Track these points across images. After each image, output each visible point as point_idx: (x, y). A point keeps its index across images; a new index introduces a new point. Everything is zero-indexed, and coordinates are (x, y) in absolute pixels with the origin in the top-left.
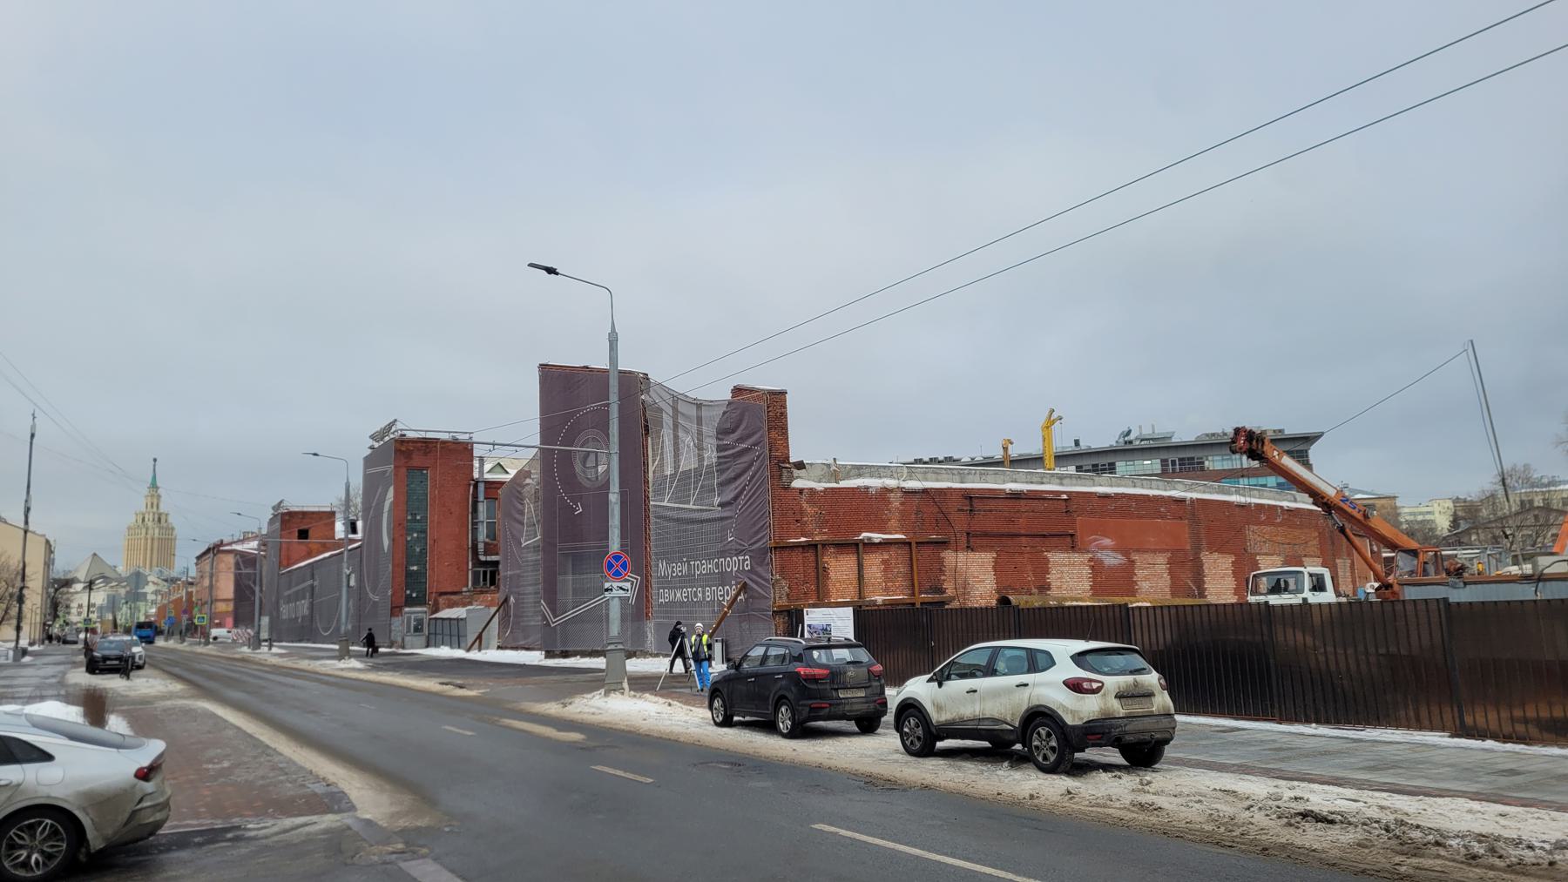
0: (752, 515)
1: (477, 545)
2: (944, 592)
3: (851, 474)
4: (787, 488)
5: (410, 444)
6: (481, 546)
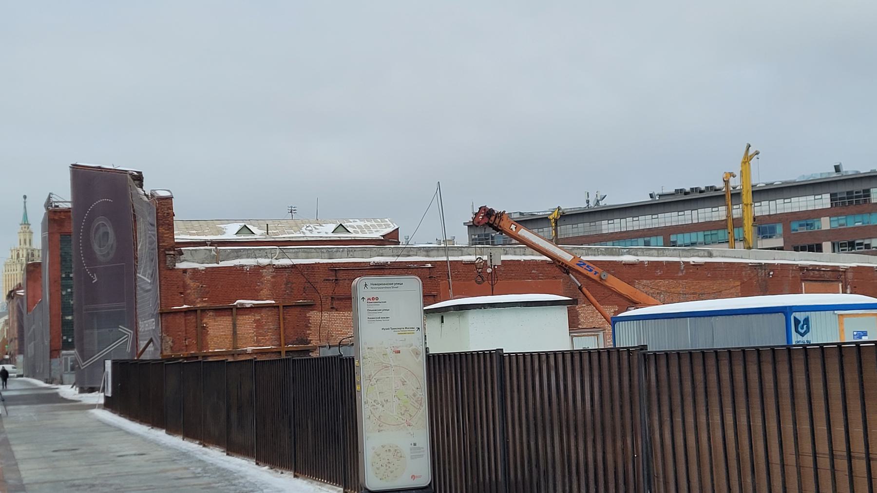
2: (309, 343)
3: (230, 256)
4: (173, 269)
5: (62, 213)
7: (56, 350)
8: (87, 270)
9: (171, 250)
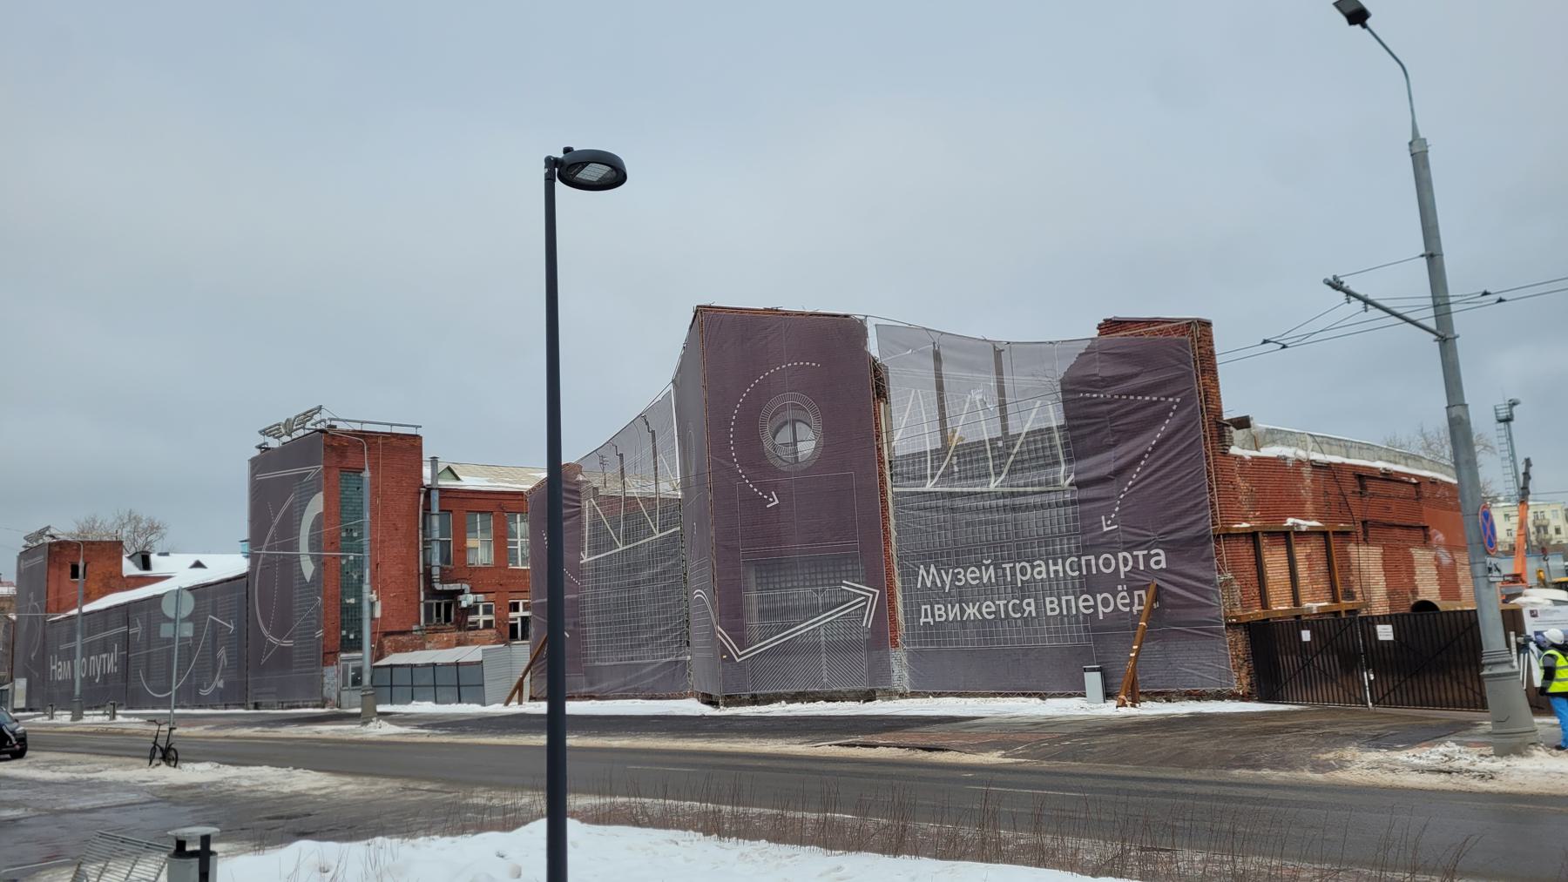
0: (1165, 492)
1: (430, 570)
6: (436, 572)
7: (331, 653)
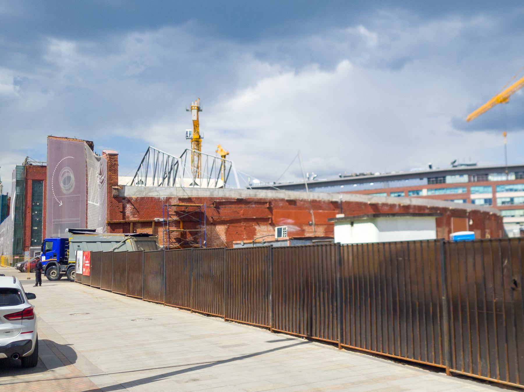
8: (56, 198)
9: (116, 186)
